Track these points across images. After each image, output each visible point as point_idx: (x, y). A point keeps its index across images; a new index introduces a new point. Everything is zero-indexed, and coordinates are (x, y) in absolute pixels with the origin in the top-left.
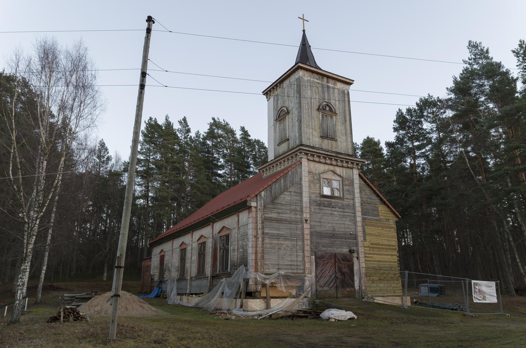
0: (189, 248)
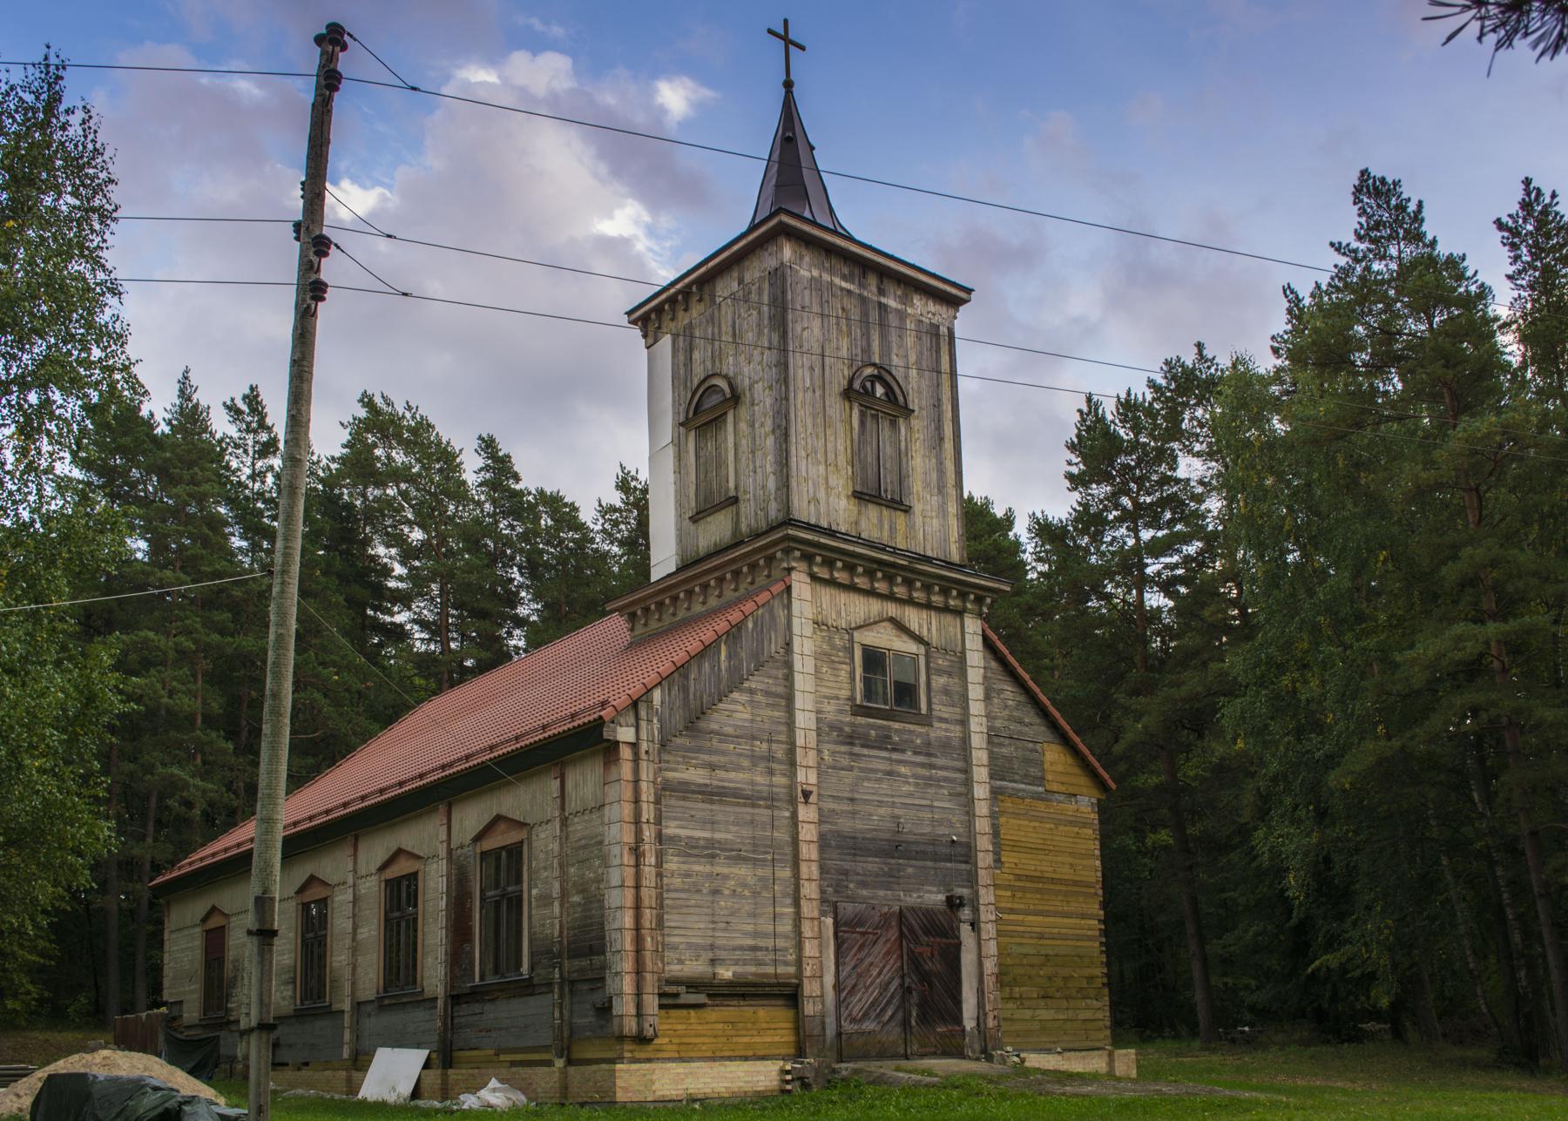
0: (342, 898)
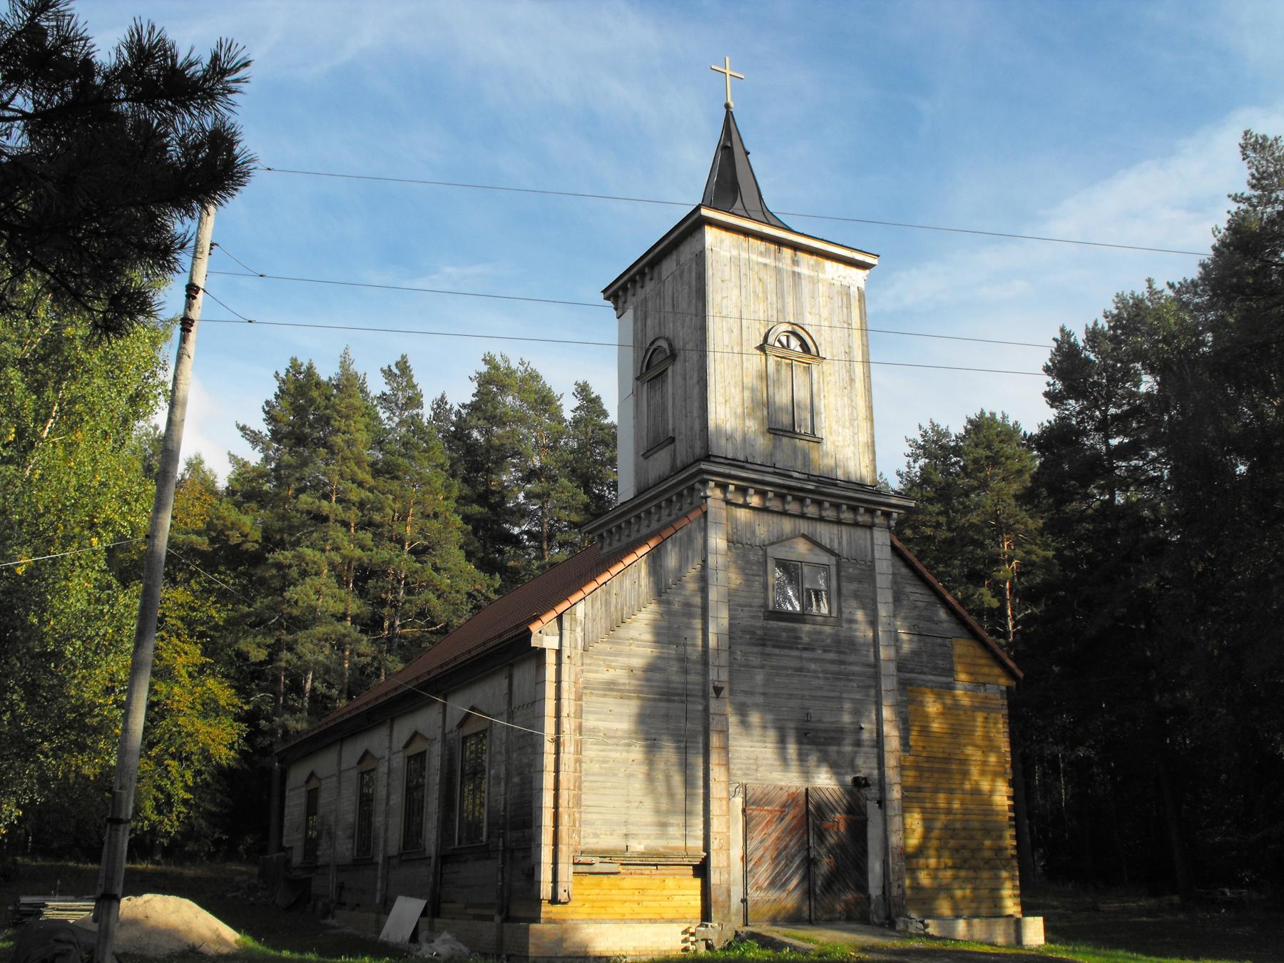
0: (383, 769)
